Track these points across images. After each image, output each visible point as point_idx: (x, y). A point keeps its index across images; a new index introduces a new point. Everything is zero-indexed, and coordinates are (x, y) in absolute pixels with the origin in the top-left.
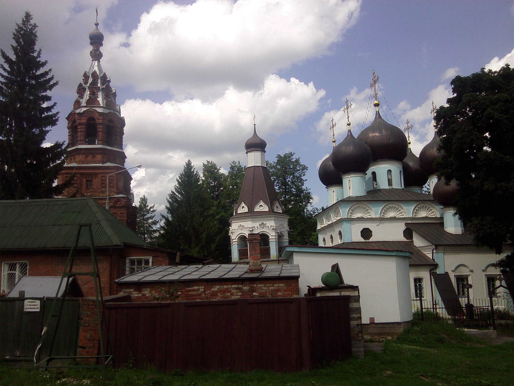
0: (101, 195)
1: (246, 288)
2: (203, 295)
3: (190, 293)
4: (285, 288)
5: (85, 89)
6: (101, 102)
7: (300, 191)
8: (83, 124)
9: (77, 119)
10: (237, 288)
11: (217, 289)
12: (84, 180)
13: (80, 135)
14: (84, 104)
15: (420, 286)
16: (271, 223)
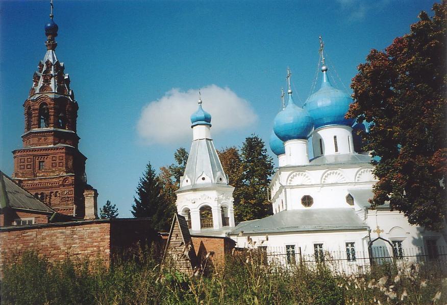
0: (51, 174)
1: (68, 232)
2: (35, 239)
3: (25, 238)
4: (99, 230)
5: (39, 77)
6: (53, 89)
7: (264, 164)
8: (37, 109)
9: (31, 105)
10: (61, 233)
11: (45, 234)
12: (37, 161)
13: (34, 120)
14: (37, 91)
15: (353, 250)
16: (213, 194)
